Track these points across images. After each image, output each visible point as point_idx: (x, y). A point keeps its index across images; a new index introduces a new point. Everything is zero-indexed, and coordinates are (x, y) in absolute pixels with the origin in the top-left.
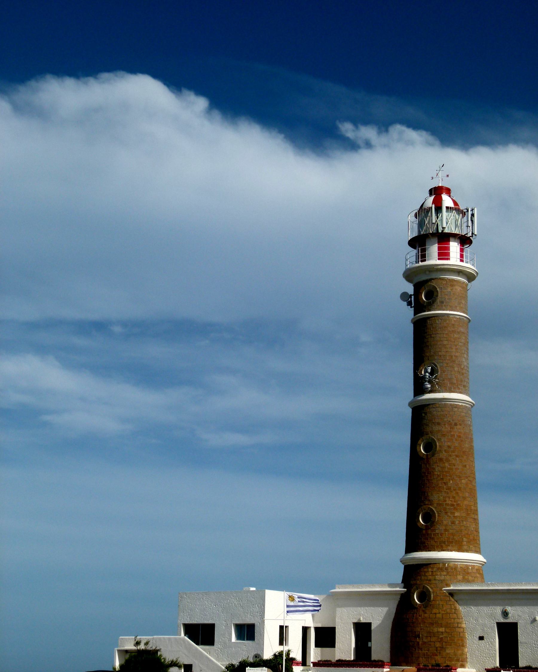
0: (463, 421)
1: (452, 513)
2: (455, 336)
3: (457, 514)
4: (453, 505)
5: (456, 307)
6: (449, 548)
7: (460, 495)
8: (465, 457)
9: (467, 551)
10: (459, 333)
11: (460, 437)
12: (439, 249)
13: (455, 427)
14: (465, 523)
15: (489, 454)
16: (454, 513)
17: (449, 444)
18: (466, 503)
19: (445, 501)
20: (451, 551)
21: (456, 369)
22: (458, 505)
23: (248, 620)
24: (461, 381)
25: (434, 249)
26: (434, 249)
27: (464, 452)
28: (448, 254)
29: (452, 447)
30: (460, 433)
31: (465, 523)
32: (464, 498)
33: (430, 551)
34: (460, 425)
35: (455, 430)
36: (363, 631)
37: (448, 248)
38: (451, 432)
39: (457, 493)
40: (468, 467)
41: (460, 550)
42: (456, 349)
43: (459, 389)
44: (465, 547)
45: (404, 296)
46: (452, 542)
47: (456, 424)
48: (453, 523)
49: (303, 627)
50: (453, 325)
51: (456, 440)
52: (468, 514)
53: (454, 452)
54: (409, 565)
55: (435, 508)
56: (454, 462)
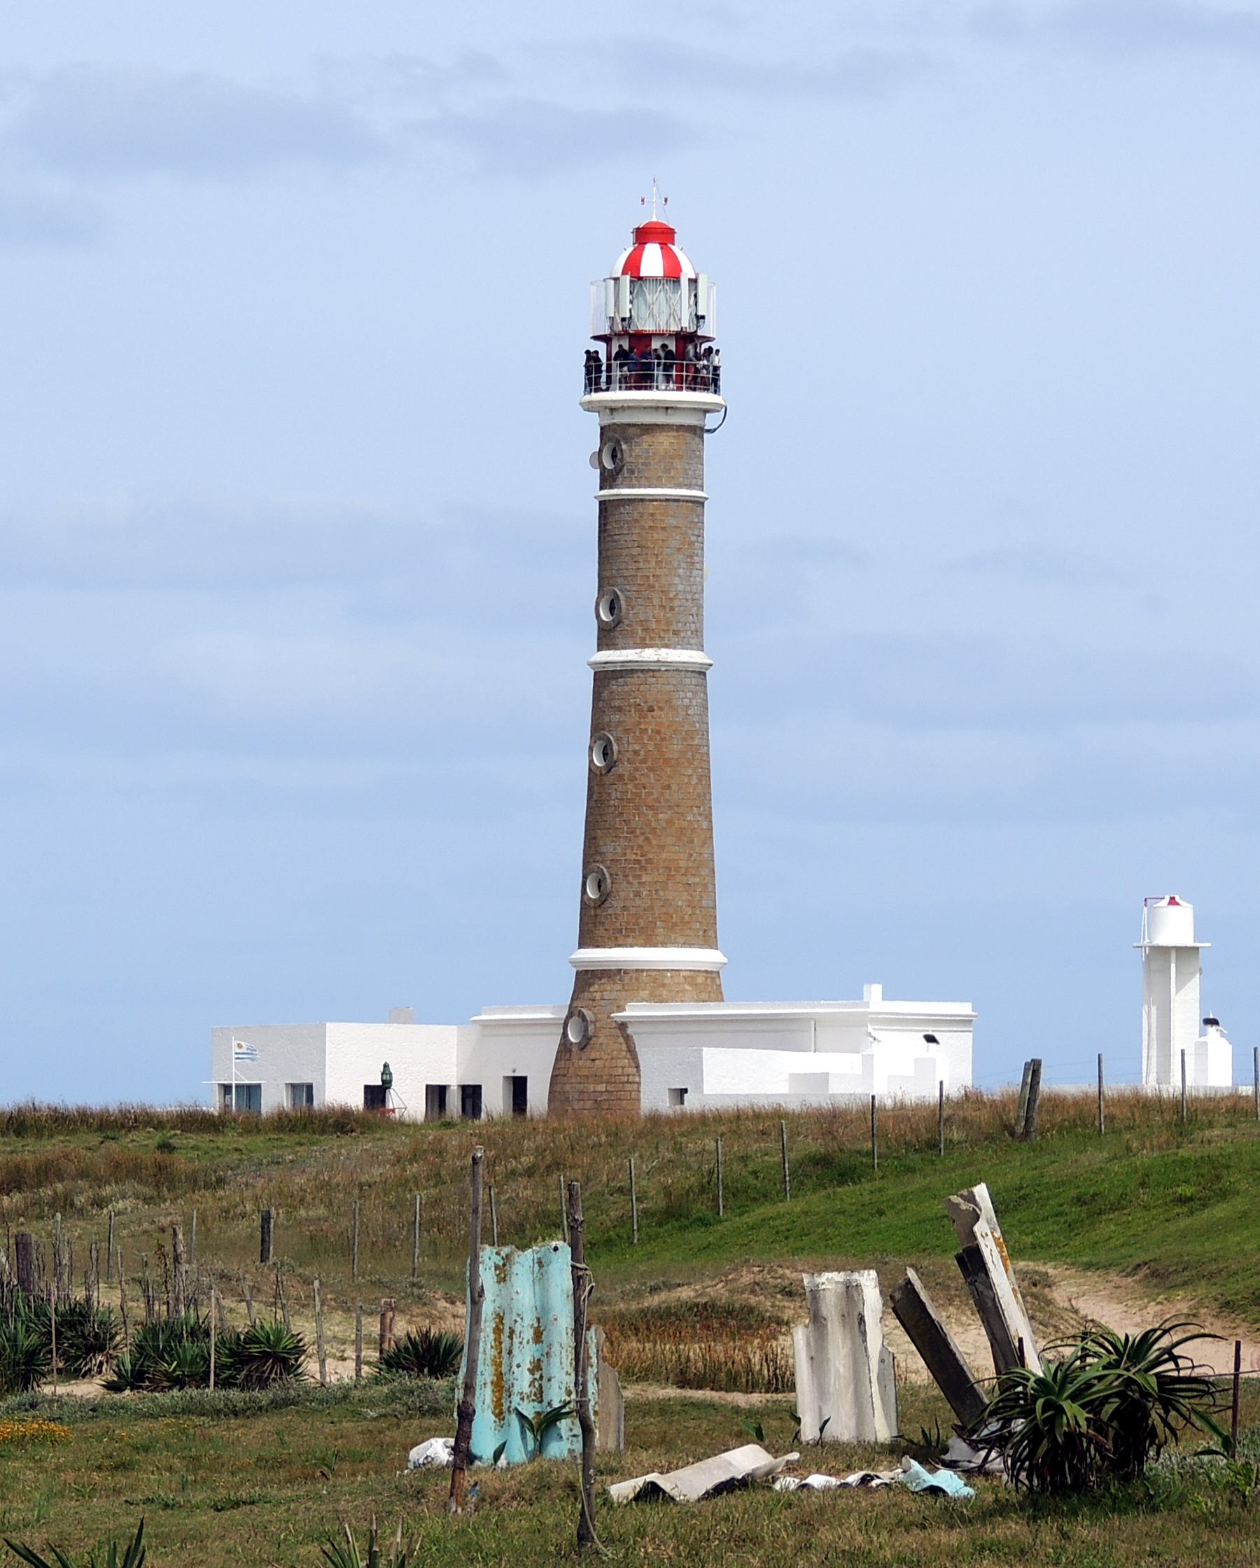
0: (668, 701)
1: (635, 876)
2: (656, 536)
4: (638, 862)
6: (630, 940)
7: (654, 842)
8: (668, 770)
11: (658, 732)
14: (661, 893)
15: (740, 750)
16: (639, 877)
17: (637, 747)
18: (664, 856)
19: (625, 854)
20: (632, 946)
21: (656, 601)
22: (649, 861)
23: (306, 1080)
24: (669, 623)
27: (667, 761)
29: (642, 753)
30: (660, 724)
31: (661, 893)
32: (662, 847)
33: (598, 947)
34: (661, 709)
35: (650, 719)
36: (518, 1086)
38: (640, 723)
40: (674, 787)
41: (649, 942)
45: (251, 1092)
46: (633, 931)
47: (651, 709)
48: (638, 894)
49: (429, 1088)
50: (652, 515)
51: (650, 739)
53: (644, 761)
55: (608, 868)
56: (644, 780)
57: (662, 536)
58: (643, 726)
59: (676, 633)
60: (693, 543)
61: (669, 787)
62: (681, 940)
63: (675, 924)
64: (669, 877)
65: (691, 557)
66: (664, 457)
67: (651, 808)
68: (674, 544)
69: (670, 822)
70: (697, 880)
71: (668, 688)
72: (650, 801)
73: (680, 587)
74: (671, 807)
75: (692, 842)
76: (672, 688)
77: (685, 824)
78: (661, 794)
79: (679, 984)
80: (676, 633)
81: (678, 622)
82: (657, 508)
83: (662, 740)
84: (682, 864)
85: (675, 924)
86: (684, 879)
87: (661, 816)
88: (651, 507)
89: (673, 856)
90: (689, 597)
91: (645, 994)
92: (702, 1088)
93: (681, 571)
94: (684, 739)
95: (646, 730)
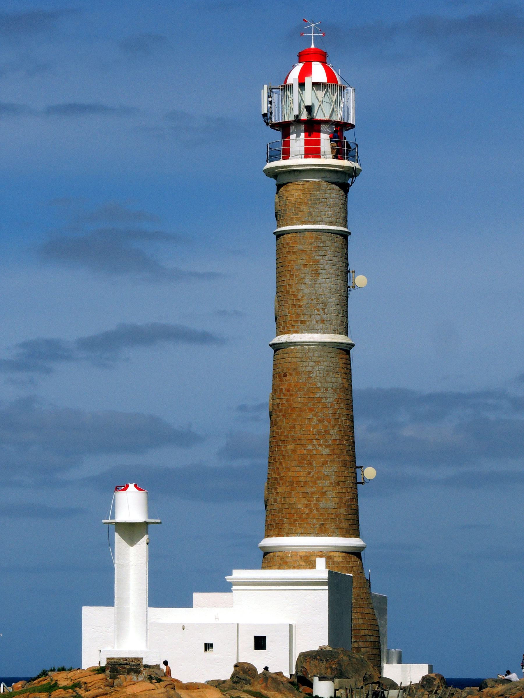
3: (279, 490)
5: (292, 219)
7: (284, 465)
9: (288, 535)
10: (294, 253)
11: (288, 390)
12: (307, 142)
13: (284, 378)
14: (287, 500)
16: (276, 489)
18: (290, 474)
21: (290, 302)
24: (298, 316)
25: (298, 142)
26: (298, 142)
27: (293, 409)
28: (318, 150)
29: (280, 405)
32: (288, 468)
37: (318, 142)
39: (281, 463)
40: (297, 427)
42: (291, 276)
43: (293, 327)
44: (286, 531)
47: (285, 375)
50: (288, 244)
52: (293, 488)
53: (281, 411)
54: (329, 605)
57: (294, 257)
58: (281, 387)
59: (303, 322)
60: (318, 261)
61: (294, 427)
62: (300, 531)
63: (296, 521)
64: (293, 488)
65: (316, 270)
66: (294, 204)
67: (283, 442)
68: (300, 262)
69: (294, 451)
70: (314, 489)
71: (295, 360)
72: (283, 438)
73: (306, 291)
74: (295, 441)
75: (311, 464)
76: (298, 360)
77: (305, 452)
78: (289, 432)
79: (296, 561)
80: (303, 322)
81: (304, 315)
82: (290, 239)
83: (291, 395)
84: (302, 479)
85: (296, 521)
86: (303, 490)
87: (289, 447)
88: (327, 219)
89: (295, 474)
90: (313, 297)
91: (277, 567)
92: (429, 667)
93: (306, 280)
94: (306, 394)
95: (282, 389)
